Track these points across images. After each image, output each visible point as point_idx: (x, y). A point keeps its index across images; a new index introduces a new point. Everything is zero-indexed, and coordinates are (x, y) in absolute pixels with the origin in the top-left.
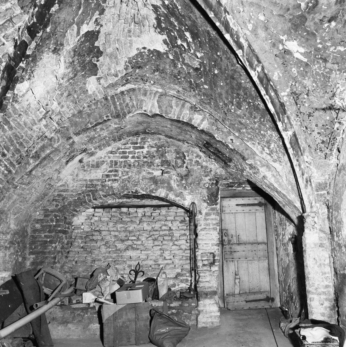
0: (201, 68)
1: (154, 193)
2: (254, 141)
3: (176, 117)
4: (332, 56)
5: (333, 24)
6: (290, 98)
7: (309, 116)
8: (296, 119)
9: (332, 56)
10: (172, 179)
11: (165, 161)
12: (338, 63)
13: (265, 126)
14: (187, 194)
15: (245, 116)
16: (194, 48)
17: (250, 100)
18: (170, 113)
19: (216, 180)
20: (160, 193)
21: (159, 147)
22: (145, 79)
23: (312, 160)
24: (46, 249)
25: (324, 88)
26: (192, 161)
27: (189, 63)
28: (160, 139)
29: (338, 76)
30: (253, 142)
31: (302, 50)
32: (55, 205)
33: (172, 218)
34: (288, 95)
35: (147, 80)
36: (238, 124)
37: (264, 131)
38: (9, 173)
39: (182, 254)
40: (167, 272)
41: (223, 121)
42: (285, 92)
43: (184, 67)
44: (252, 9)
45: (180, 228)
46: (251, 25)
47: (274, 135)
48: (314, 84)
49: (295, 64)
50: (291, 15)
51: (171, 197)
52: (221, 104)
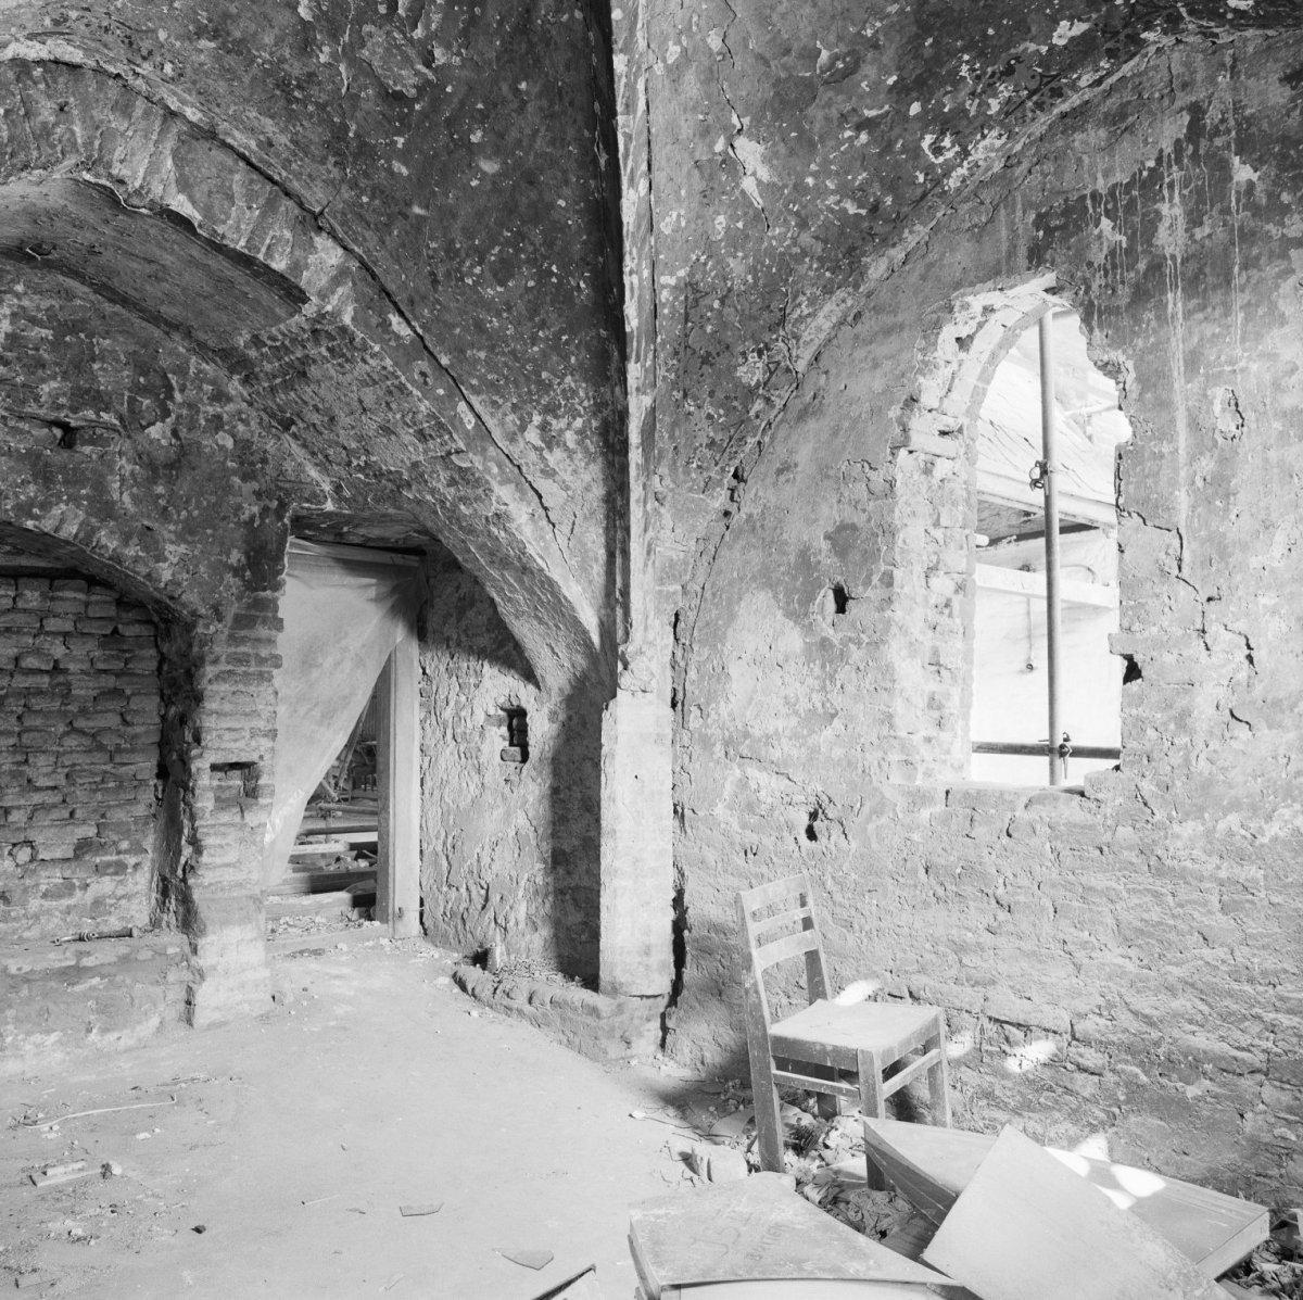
0: (416, 100)
1: (36, 518)
2: (502, 397)
3: (242, 243)
4: (822, 218)
5: (864, 137)
6: (676, 298)
7: (703, 363)
8: (671, 363)
9: (822, 218)
10: (112, 471)
11: (87, 391)
12: (825, 242)
13: (566, 358)
14: (173, 537)
15: (509, 310)
16: (434, 26)
17: (554, 268)
18: (224, 222)
19: (279, 499)
20: (62, 521)
21: (65, 327)
22: (146, 45)
23: (672, 490)
25: (767, 296)
26: (198, 412)
27: (376, 63)
28: (69, 295)
29: (811, 273)
30: (495, 398)
31: (764, 174)
33: (68, 626)
34: (675, 287)
35: (150, 53)
36: (465, 329)
37: (553, 372)
39: (104, 767)
40: (39, 839)
41: (412, 302)
42: (672, 274)
43: (342, 68)
44: (704, 7)
45: (101, 666)
46: (678, 48)
47: (582, 394)
48: (750, 277)
49: (734, 205)
50: (785, 67)
51: (104, 541)
52: (433, 245)
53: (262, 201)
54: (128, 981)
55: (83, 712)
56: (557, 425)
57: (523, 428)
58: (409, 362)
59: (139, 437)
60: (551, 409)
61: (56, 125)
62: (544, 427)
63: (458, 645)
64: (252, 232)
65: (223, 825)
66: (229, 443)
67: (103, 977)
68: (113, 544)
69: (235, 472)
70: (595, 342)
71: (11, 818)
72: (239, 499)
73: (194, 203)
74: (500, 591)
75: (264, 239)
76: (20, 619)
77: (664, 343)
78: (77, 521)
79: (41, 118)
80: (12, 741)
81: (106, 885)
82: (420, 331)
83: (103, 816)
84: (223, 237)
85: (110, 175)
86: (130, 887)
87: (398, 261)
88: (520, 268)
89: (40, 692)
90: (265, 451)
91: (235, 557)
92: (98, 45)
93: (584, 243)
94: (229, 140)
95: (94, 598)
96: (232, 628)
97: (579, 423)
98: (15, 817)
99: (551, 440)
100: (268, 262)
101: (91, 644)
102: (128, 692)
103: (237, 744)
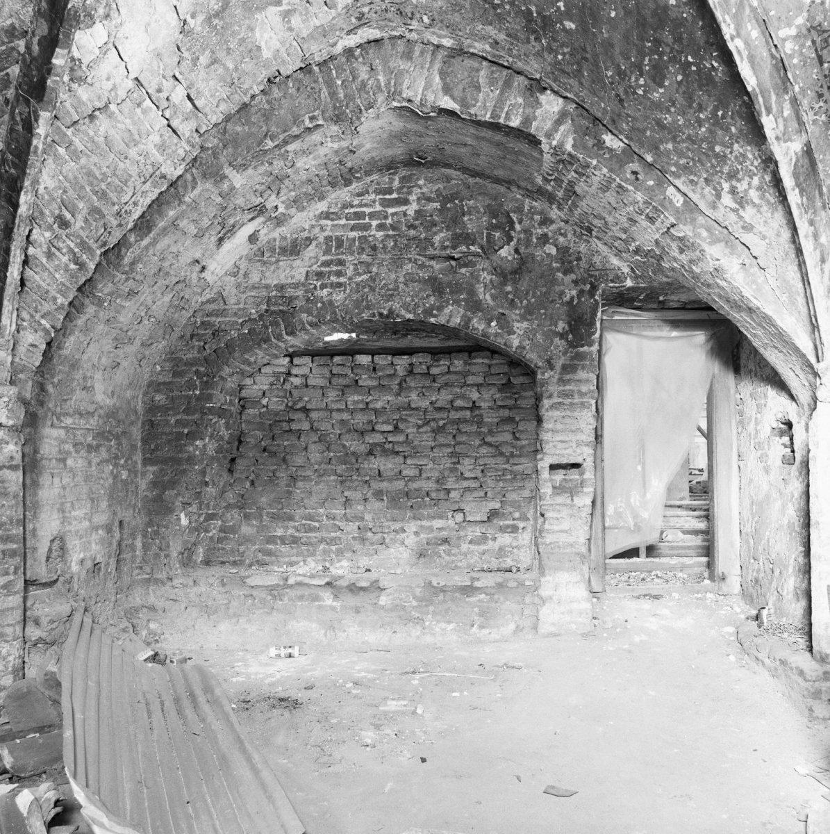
1: (435, 316)
2: (696, 175)
3: (488, 115)
6: (802, 46)
10: (478, 282)
11: (461, 235)
13: (727, 130)
14: (518, 318)
15: (674, 105)
17: (690, 58)
18: (474, 106)
19: (591, 283)
20: (451, 316)
24: (181, 451)
26: (531, 234)
28: (448, 179)
30: (692, 177)
32: (196, 348)
33: (480, 380)
34: (798, 36)
35: (413, 14)
36: (653, 130)
37: (723, 144)
38: (79, 269)
40: (467, 509)
41: (614, 121)
42: (789, 25)
45: (500, 403)
47: (750, 156)
51: (476, 325)
52: (610, 74)
53: (500, 83)
54: (502, 599)
55: (491, 432)
56: (742, 187)
57: (718, 196)
58: (621, 166)
59: (494, 258)
60: (732, 176)
61: (369, 79)
62: (733, 191)
63: (756, 375)
64: (495, 106)
65: (559, 505)
66: (554, 251)
67: (487, 594)
68: (481, 327)
69: (558, 270)
70: (744, 109)
71: (451, 495)
72: (562, 288)
73: (453, 98)
74: (747, 329)
75: (503, 109)
76: (453, 378)
77: (803, 90)
78: (460, 315)
79: (360, 79)
80: (450, 450)
81: (505, 539)
82: (626, 141)
83: (504, 496)
84: (476, 115)
85: (404, 99)
86: (521, 542)
87: (595, 94)
88: (667, 68)
89: (466, 421)
90: (579, 252)
91: (561, 326)
92: (386, 22)
93: (702, 28)
94: (472, 50)
95: (494, 362)
96: (561, 374)
97: (756, 181)
98: (453, 494)
99: (742, 201)
100: (507, 123)
101: (493, 390)
102: (517, 419)
103: (567, 451)
